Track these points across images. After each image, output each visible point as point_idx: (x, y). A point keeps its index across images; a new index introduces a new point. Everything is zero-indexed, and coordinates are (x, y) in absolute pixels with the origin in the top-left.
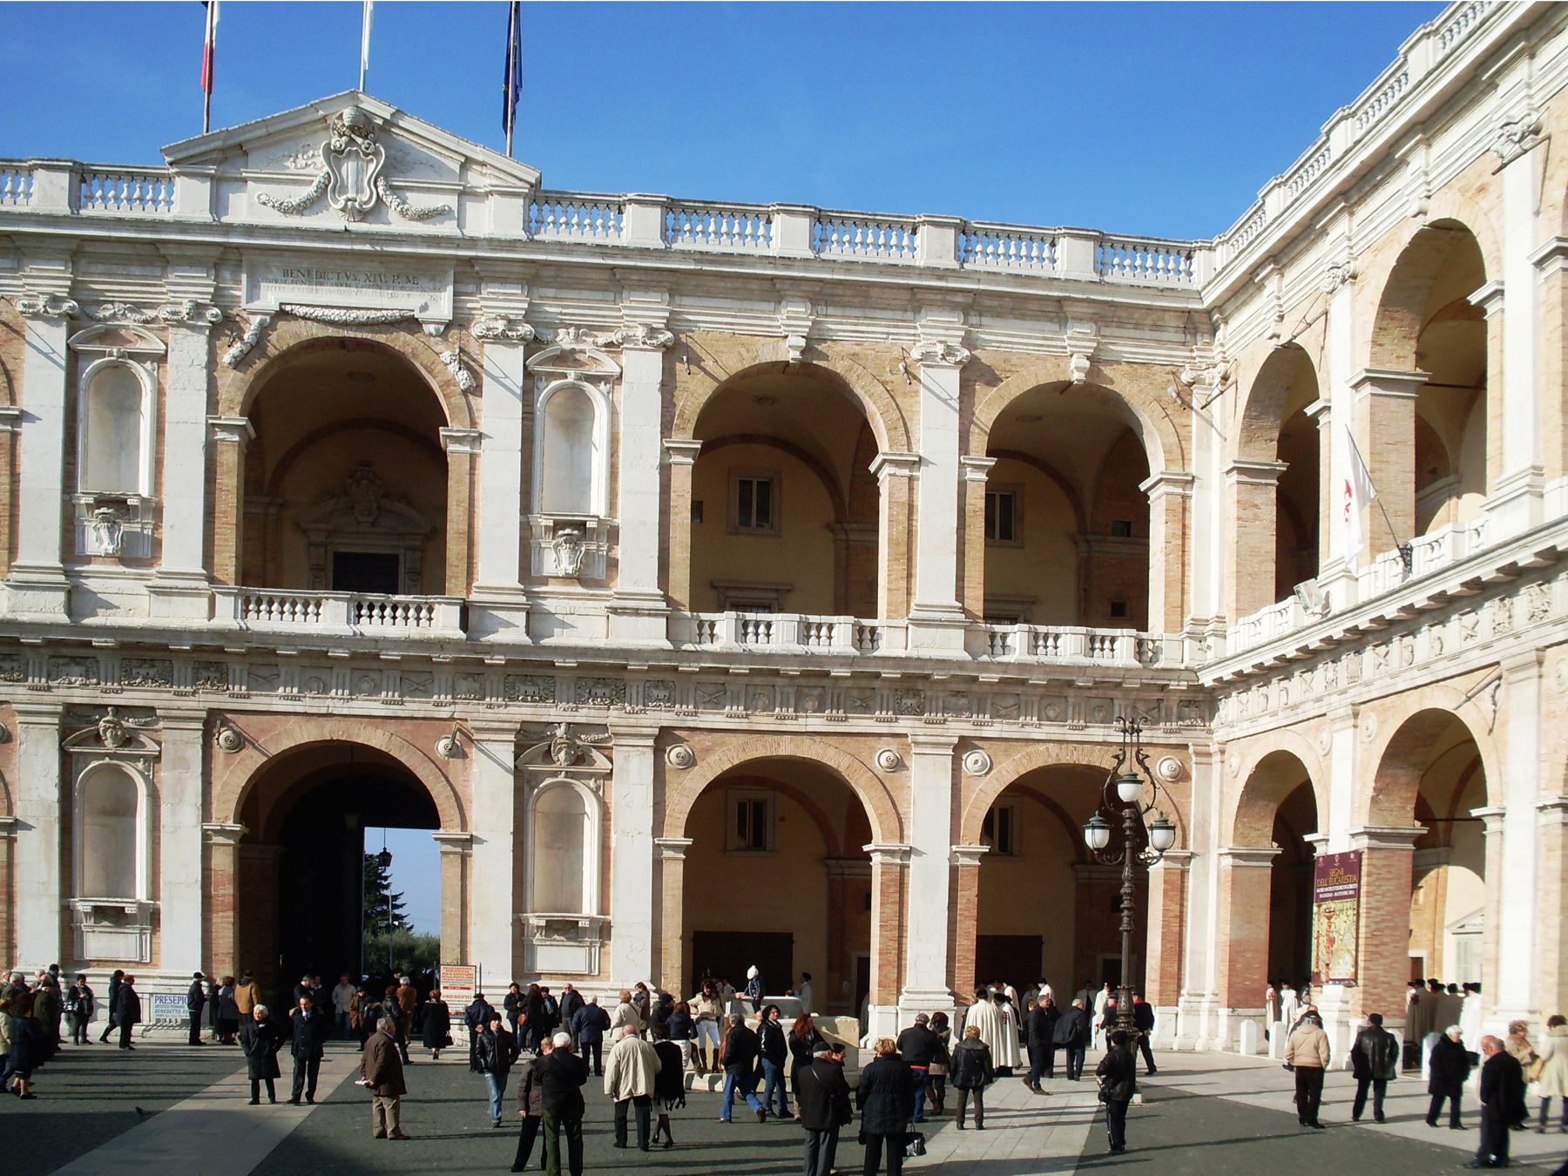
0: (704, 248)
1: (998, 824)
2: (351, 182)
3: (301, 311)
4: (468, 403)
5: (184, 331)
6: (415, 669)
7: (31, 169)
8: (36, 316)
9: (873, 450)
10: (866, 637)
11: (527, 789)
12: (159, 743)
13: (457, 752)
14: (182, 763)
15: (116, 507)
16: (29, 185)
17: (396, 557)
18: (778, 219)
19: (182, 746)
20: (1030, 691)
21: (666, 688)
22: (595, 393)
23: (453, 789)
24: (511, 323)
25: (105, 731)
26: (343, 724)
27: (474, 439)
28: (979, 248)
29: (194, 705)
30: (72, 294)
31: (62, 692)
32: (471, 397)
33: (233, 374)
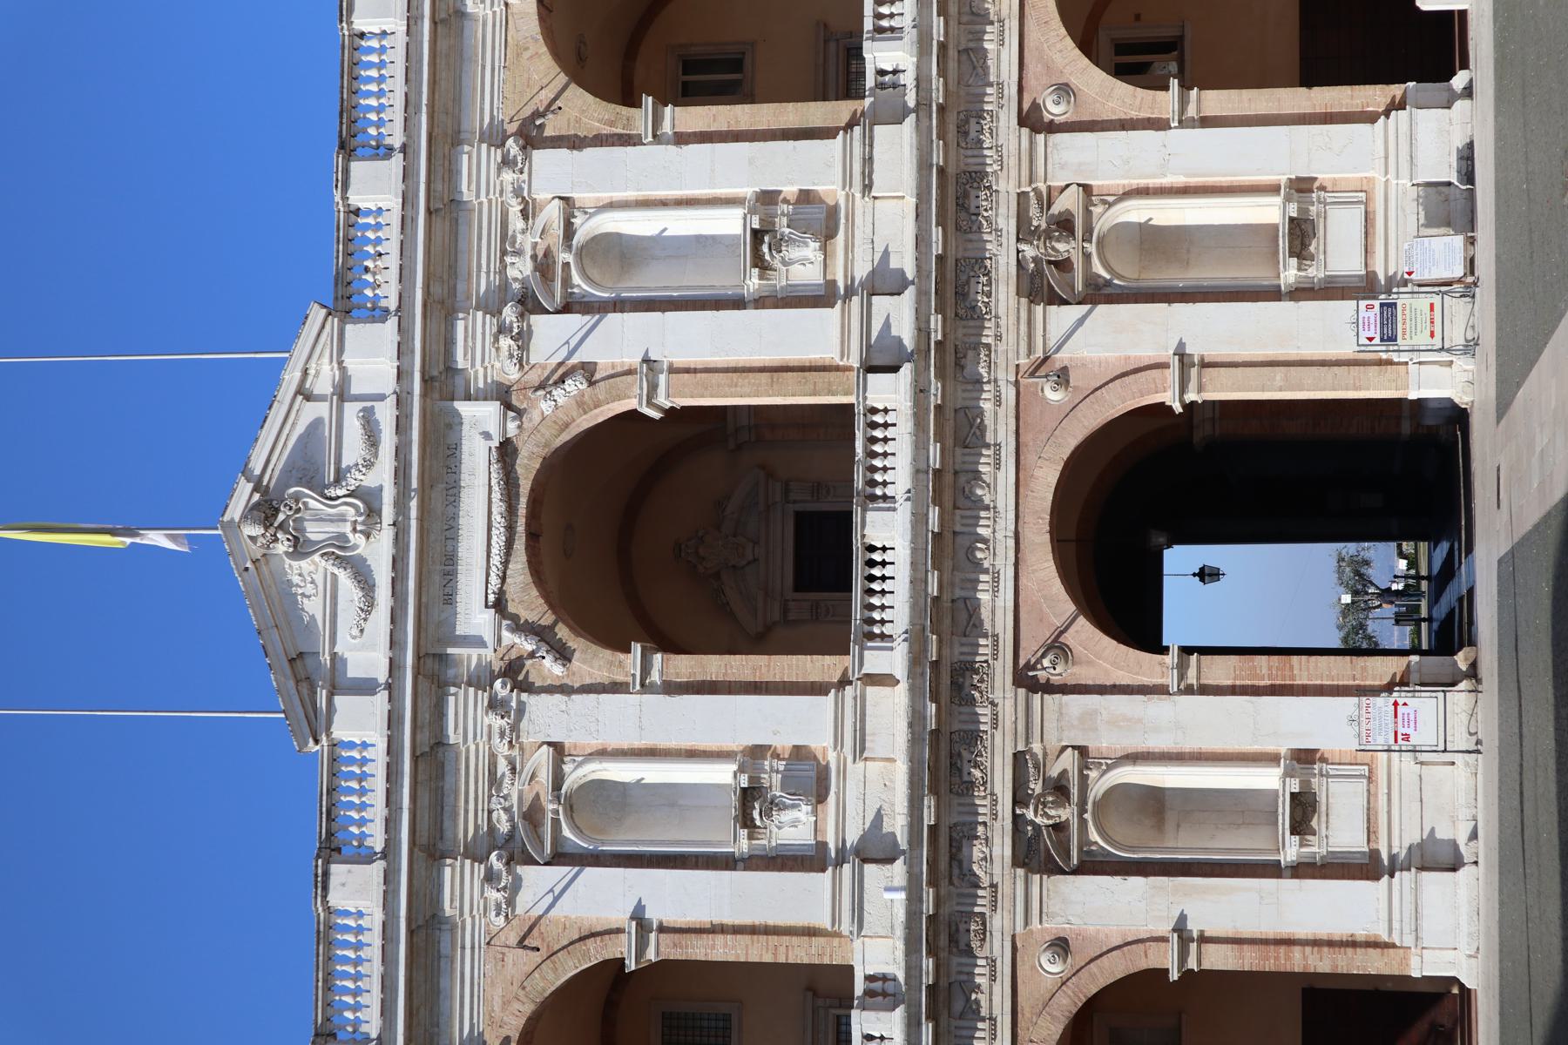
0: (378, 928)
1: (1133, 61)
2: (333, 529)
3: (495, 581)
4: (603, 379)
5: (524, 724)
6: (956, 430)
7: (328, 910)
8: (511, 902)
9: (633, 415)
10: (882, 993)
11: (1108, 291)
12: (1064, 748)
13: (1062, 377)
14: (1089, 717)
15: (750, 801)
16: (347, 914)
17: (800, 517)
18: (360, 24)
19: (1066, 721)
20: (951, 337)
21: (967, 122)
22: (586, 228)
23: (1112, 380)
24: (502, 330)
25: (1049, 817)
26: (1027, 517)
27: (650, 369)
28: (372, 131)
29: (1009, 703)
30: (482, 859)
31: (997, 870)
32: (597, 376)
33: (576, 663)
